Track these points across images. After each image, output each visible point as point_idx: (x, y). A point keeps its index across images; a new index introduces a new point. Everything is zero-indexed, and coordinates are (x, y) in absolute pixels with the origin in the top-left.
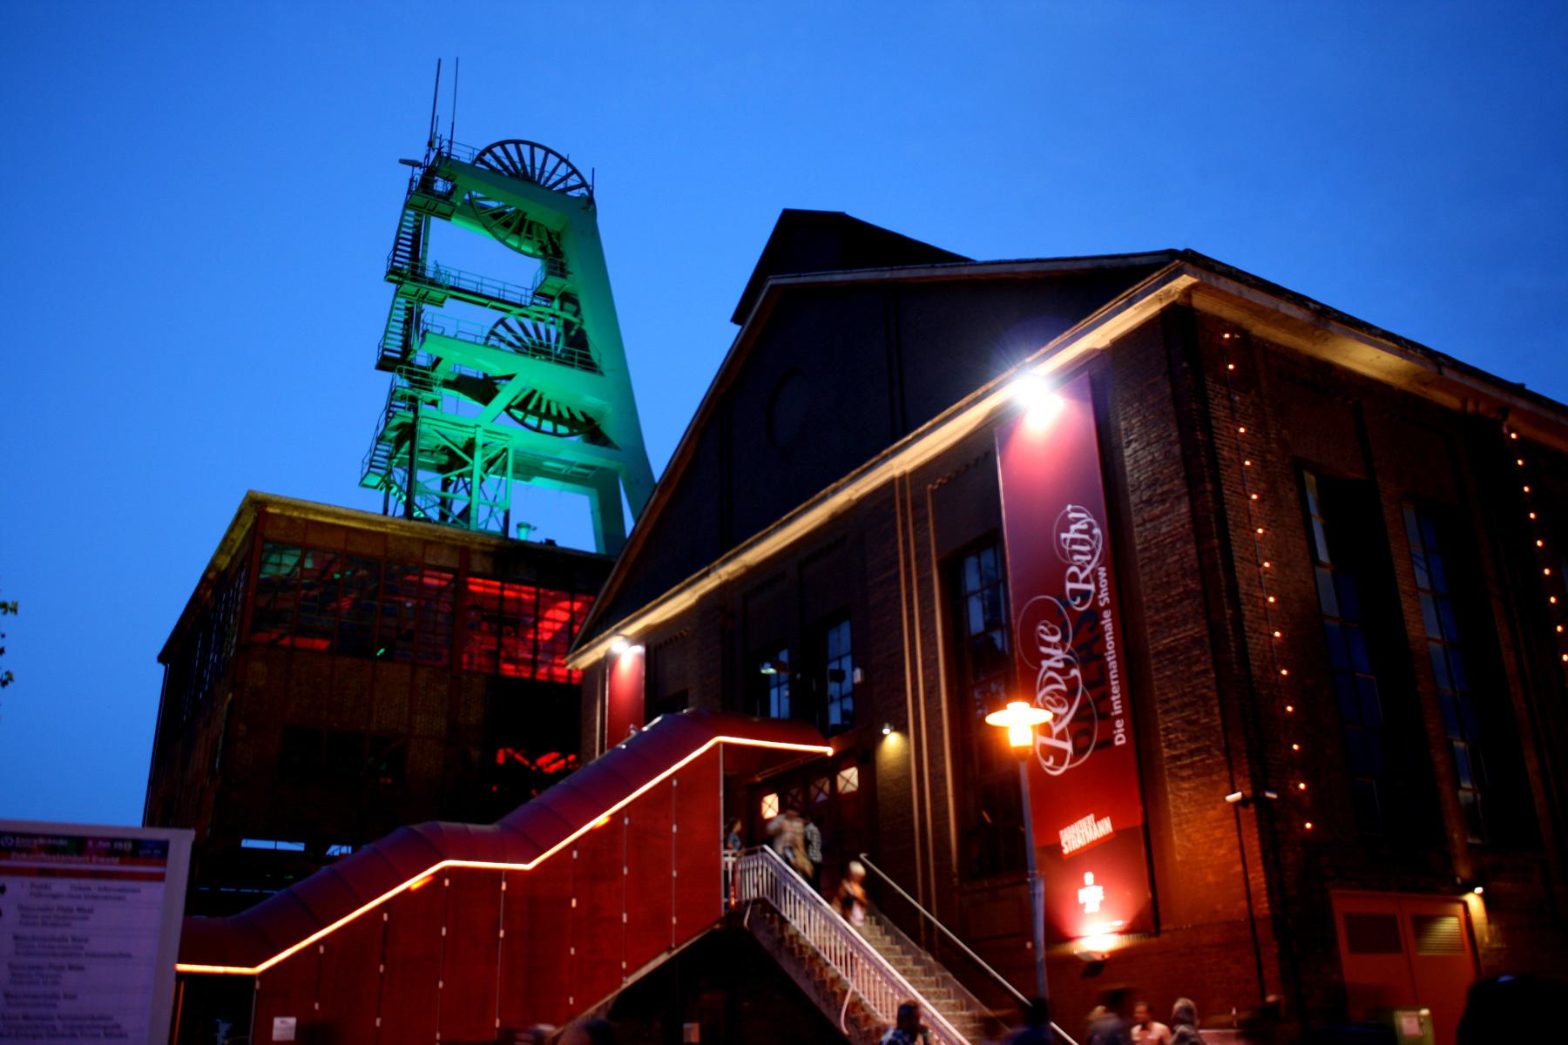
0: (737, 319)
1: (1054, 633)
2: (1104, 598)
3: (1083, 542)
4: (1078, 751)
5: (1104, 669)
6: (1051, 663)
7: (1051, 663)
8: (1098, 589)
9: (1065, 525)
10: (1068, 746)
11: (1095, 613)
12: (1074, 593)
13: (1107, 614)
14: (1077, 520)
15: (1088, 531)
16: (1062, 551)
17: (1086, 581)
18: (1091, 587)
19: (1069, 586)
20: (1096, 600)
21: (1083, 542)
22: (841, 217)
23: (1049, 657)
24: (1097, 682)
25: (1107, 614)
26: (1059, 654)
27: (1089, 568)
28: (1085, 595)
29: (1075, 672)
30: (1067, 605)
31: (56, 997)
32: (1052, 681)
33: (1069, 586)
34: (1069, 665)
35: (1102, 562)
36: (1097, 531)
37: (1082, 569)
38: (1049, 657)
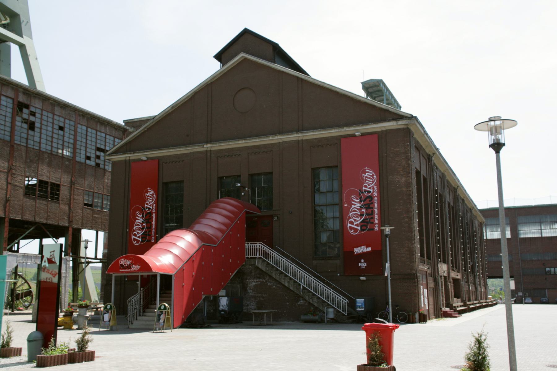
0: (218, 57)
1: (357, 199)
2: (154, 211)
3: (370, 178)
4: (142, 241)
5: (151, 225)
6: (355, 206)
7: (355, 206)
8: (373, 192)
9: (147, 192)
10: (140, 240)
11: (151, 213)
12: (147, 208)
13: (154, 214)
14: (368, 172)
15: (153, 195)
16: (363, 179)
17: (150, 206)
18: (372, 190)
19: (146, 205)
20: (152, 211)
21: (370, 178)
22: (277, 45)
23: (355, 205)
24: (149, 228)
25: (154, 214)
26: (141, 219)
27: (371, 186)
28: (149, 209)
29: (144, 224)
30: (144, 209)
31: (27, 147)
32: (138, 225)
33: (146, 205)
34: (143, 223)
35: (155, 203)
36: (154, 196)
37: (369, 185)
38: (355, 205)
